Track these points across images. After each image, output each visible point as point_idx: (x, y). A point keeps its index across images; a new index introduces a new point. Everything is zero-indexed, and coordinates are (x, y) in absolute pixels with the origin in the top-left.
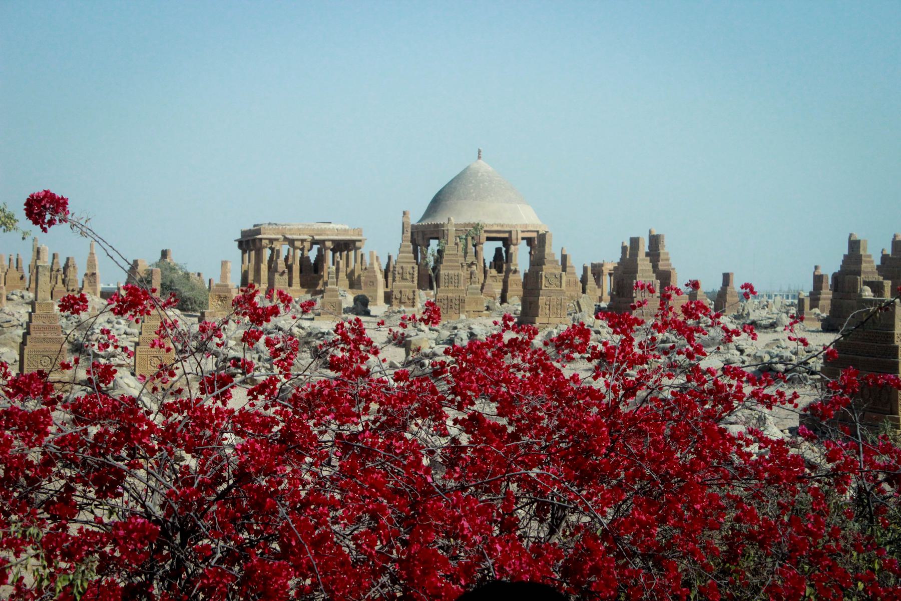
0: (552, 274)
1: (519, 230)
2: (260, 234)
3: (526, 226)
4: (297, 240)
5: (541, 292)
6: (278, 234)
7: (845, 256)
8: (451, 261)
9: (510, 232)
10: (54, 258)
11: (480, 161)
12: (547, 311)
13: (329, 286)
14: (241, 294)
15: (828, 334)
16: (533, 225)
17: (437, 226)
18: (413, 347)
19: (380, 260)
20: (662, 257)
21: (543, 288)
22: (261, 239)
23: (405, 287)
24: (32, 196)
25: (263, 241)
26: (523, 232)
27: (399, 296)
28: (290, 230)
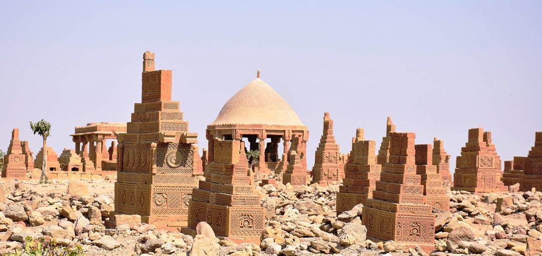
0: (485, 157)
1: (240, 132)
2: (96, 130)
3: (295, 127)
4: (100, 134)
5: (478, 170)
6: (109, 130)
7: (530, 152)
8: (331, 146)
9: (284, 131)
10: (258, 74)
11: (259, 79)
12: (483, 183)
13: (295, 165)
14: (114, 175)
15: (438, 225)
16: (299, 127)
17: (230, 126)
18: (24, 239)
19: (33, 156)
20: (441, 151)
21: (480, 167)
22: (97, 135)
23: (331, 167)
24: (209, 127)
25: (99, 136)
26: (266, 131)
27: (326, 173)
28: (119, 128)
